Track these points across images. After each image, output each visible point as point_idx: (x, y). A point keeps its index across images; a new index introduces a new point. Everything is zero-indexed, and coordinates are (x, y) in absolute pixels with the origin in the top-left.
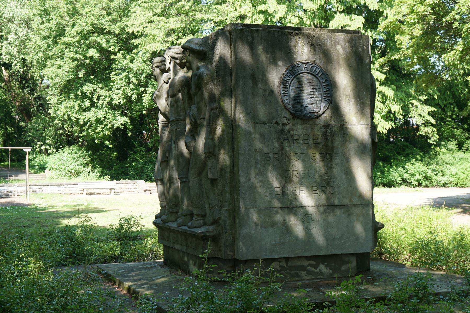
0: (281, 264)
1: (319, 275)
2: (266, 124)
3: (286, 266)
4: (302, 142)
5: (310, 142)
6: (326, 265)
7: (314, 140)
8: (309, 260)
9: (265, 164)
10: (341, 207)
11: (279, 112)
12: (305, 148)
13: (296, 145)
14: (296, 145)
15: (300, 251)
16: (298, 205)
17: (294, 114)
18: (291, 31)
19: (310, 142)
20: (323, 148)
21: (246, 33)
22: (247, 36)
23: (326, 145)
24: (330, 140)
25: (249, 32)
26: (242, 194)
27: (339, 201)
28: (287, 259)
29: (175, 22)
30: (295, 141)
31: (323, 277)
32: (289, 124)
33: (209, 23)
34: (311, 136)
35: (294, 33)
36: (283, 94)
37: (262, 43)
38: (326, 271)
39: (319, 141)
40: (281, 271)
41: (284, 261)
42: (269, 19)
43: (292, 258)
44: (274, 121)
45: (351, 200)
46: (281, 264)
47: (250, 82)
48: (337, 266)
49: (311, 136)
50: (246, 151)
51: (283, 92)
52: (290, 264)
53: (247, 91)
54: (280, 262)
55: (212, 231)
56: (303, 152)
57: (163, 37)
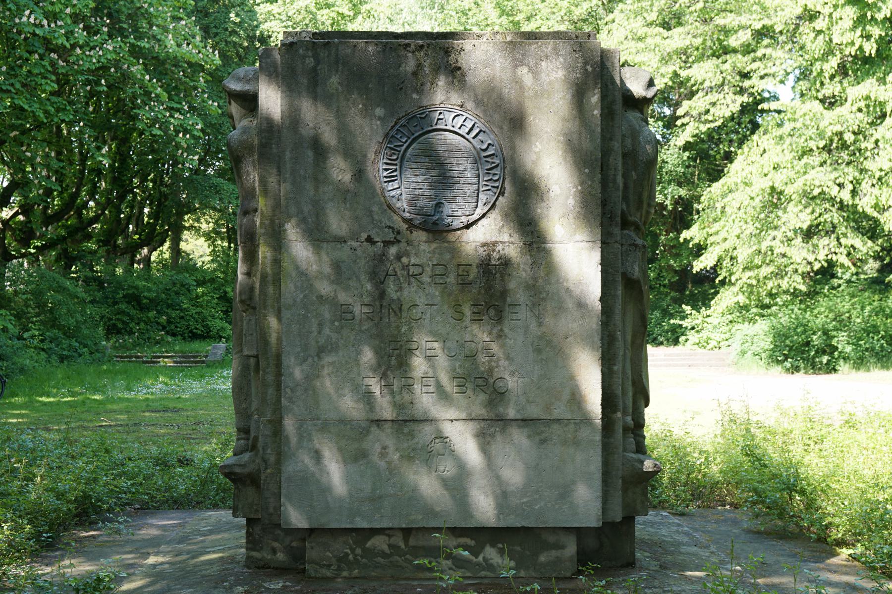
0: (393, 540)
1: (484, 570)
2: (345, 242)
3: (403, 546)
4: (429, 280)
5: (448, 280)
6: (499, 548)
7: (458, 275)
8: (461, 536)
9: (342, 328)
10: (522, 423)
11: (376, 217)
12: (437, 293)
13: (414, 287)
14: (414, 287)
15: (420, 517)
16: (419, 415)
17: (411, 220)
18: (407, 41)
19: (448, 280)
20: (479, 293)
21: (301, 51)
22: (304, 57)
23: (489, 288)
24: (498, 275)
25: (307, 49)
26: (288, 390)
27: (518, 411)
28: (407, 532)
29: (683, 36)
30: (412, 279)
31: (492, 575)
32: (399, 241)
33: (741, 33)
34: (451, 267)
35: (412, 46)
36: (386, 177)
37: (337, 71)
38: (500, 561)
39: (471, 277)
40: (391, 555)
41: (400, 534)
42: (869, 14)
43: (317, 529)
44: (364, 236)
45: (548, 408)
46: (393, 540)
47: (310, 153)
48: (528, 553)
49: (451, 267)
50: (298, 300)
51: (385, 173)
52: (412, 542)
53: (302, 172)
54: (390, 536)
55: (247, 464)
56: (431, 303)
57: (655, 66)
